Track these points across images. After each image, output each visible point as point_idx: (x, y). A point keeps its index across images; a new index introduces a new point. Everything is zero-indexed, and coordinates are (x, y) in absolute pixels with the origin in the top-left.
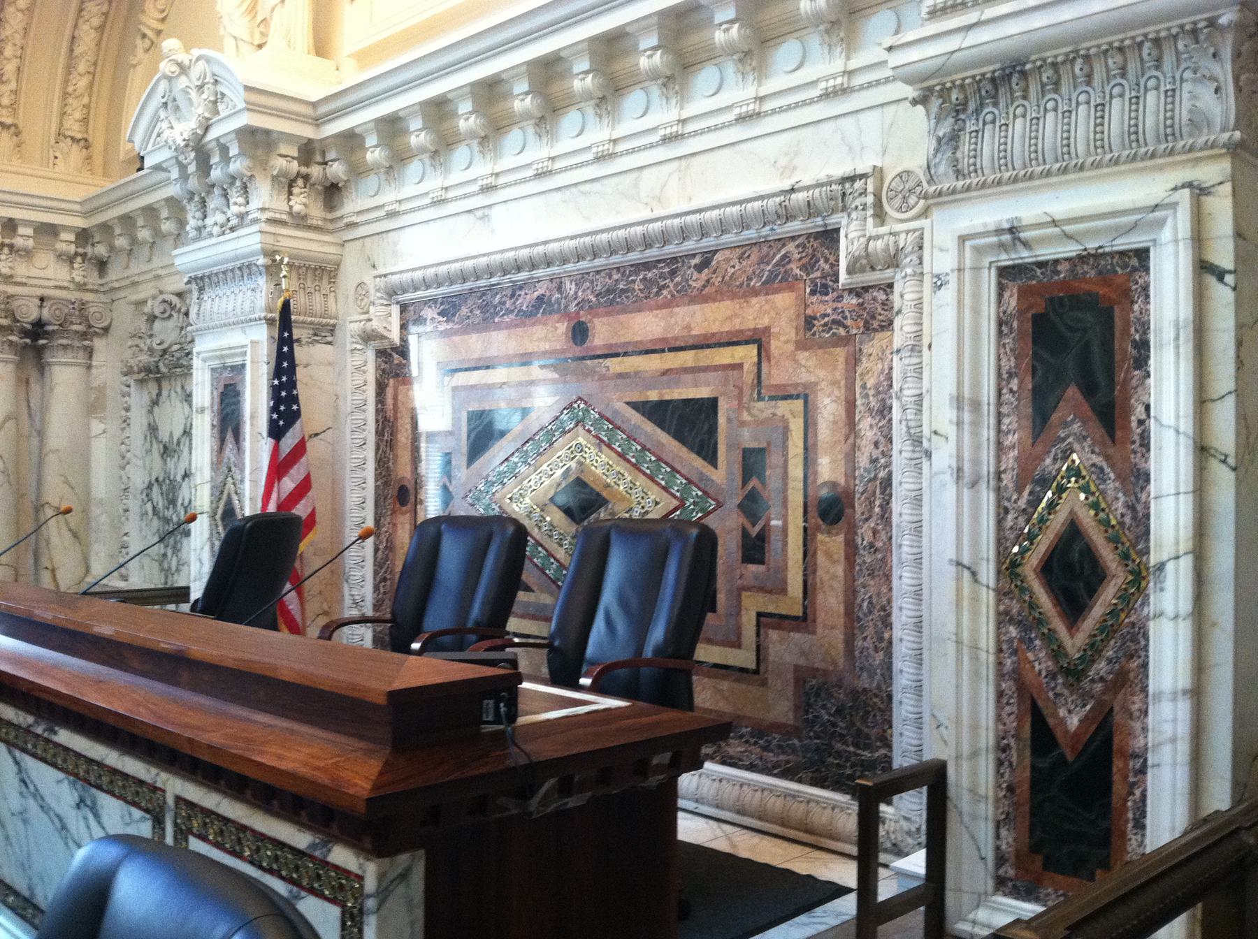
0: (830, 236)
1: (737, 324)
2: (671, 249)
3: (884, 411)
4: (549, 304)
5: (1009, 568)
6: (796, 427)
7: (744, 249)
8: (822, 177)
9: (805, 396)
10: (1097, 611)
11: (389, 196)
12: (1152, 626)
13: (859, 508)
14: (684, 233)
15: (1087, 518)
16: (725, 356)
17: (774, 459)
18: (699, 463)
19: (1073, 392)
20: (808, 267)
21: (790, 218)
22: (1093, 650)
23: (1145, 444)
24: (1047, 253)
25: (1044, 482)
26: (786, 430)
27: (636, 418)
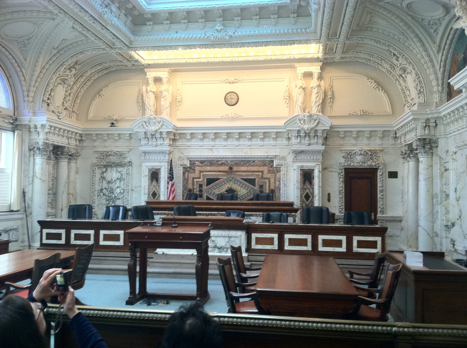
0: (272, 161)
1: (258, 170)
2: (248, 159)
3: (279, 181)
4: (225, 164)
5: (301, 197)
6: (268, 182)
7: (260, 161)
8: (273, 155)
9: (269, 179)
10: (310, 200)
11: (189, 144)
12: (315, 201)
13: (276, 191)
14: (252, 158)
15: (309, 192)
16: (257, 173)
17: (264, 186)
18: (252, 186)
19: (307, 181)
20: (269, 164)
21: (267, 158)
22: (309, 204)
23: (314, 186)
24: (305, 168)
25: (305, 189)
26: (266, 183)
27: (242, 180)
